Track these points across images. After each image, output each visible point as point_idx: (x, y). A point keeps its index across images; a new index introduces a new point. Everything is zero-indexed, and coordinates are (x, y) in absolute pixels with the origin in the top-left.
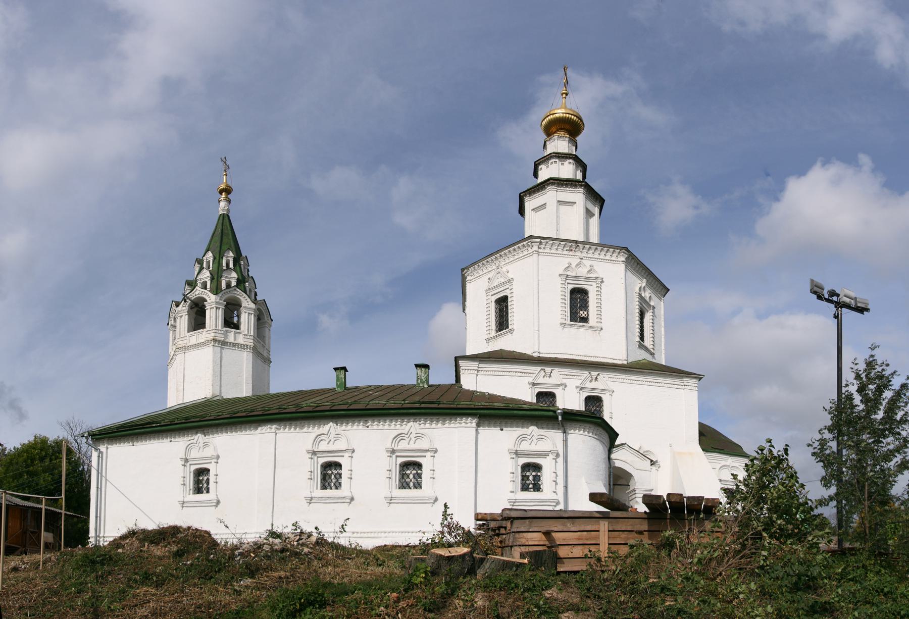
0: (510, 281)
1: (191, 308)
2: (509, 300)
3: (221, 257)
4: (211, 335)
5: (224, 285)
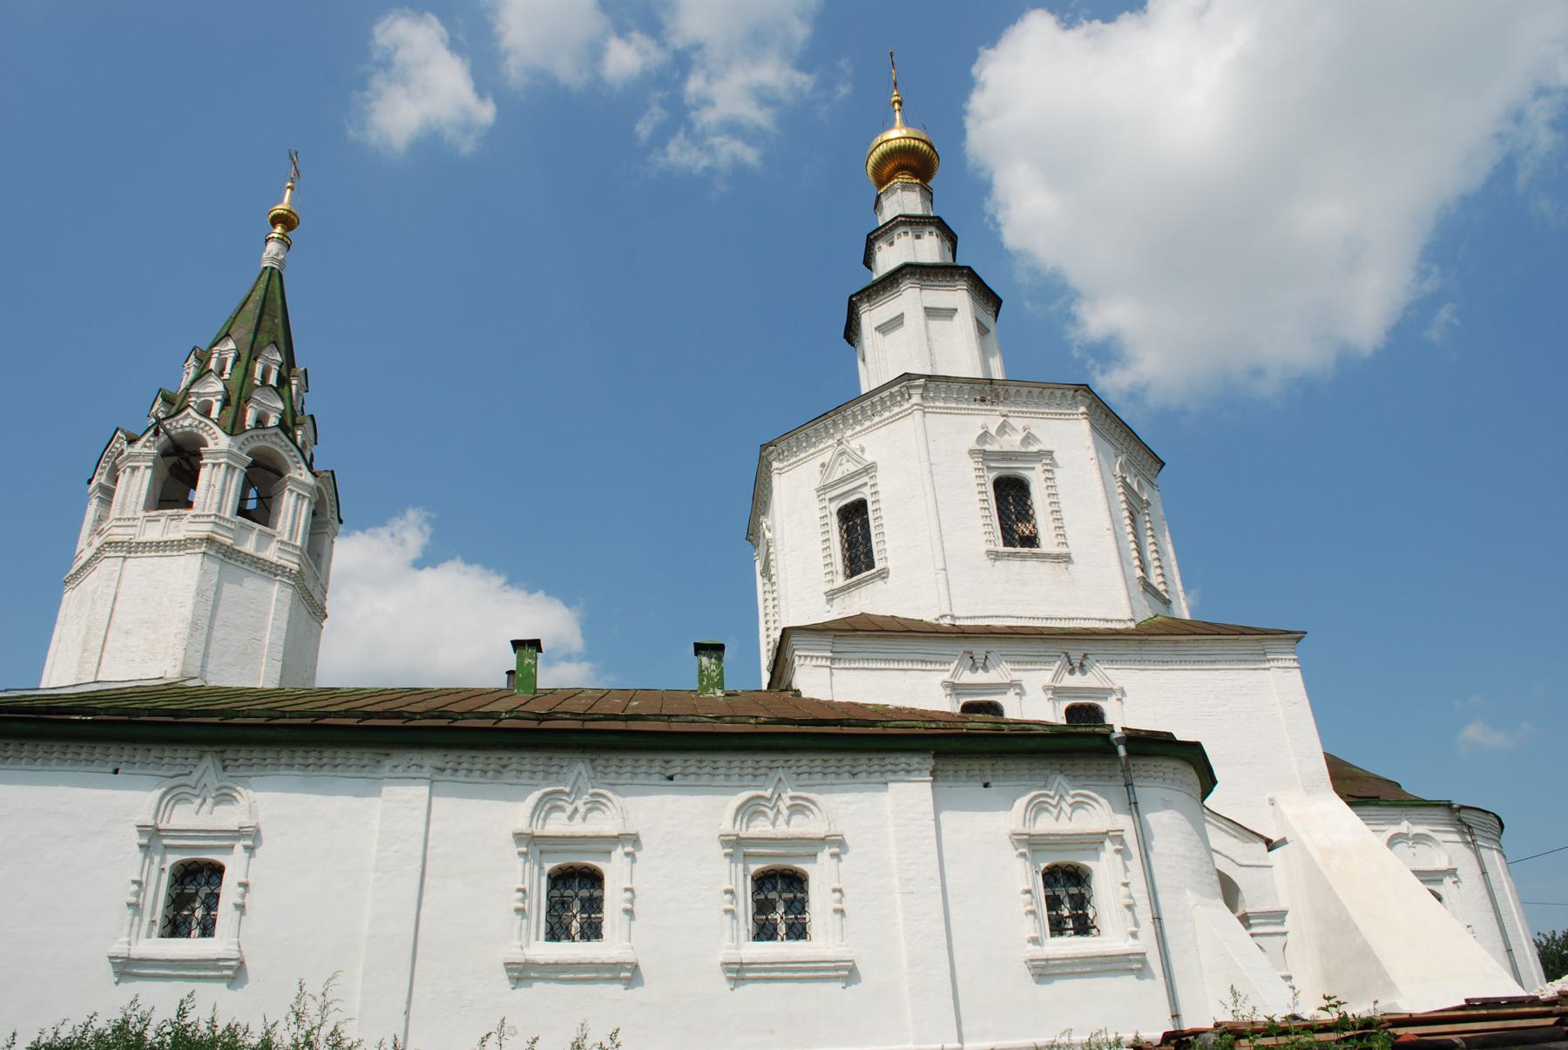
0: (869, 469)
1: (165, 454)
3: (254, 355)
4: (203, 529)
5: (250, 419)
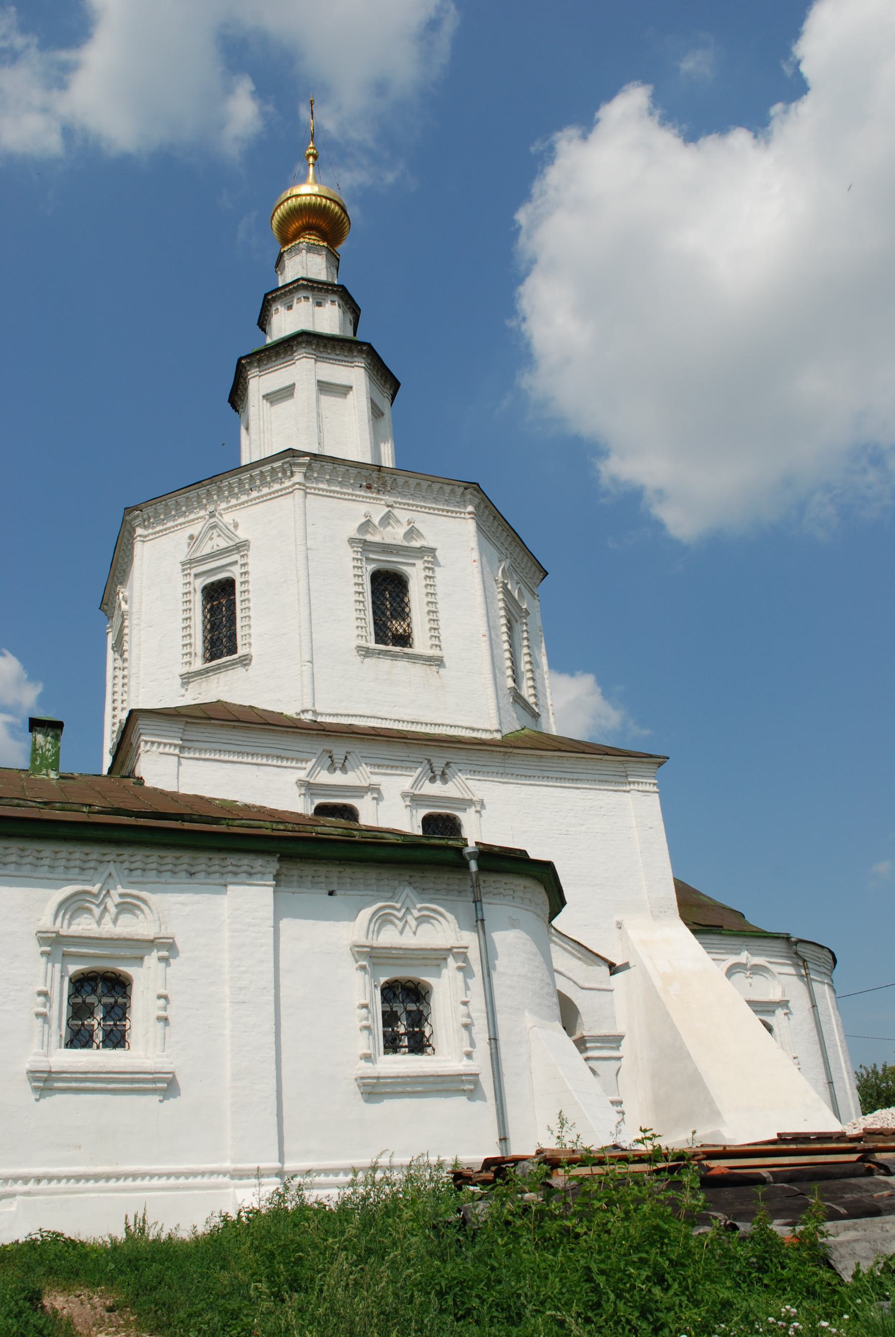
0: (241, 547)
2: (238, 588)
